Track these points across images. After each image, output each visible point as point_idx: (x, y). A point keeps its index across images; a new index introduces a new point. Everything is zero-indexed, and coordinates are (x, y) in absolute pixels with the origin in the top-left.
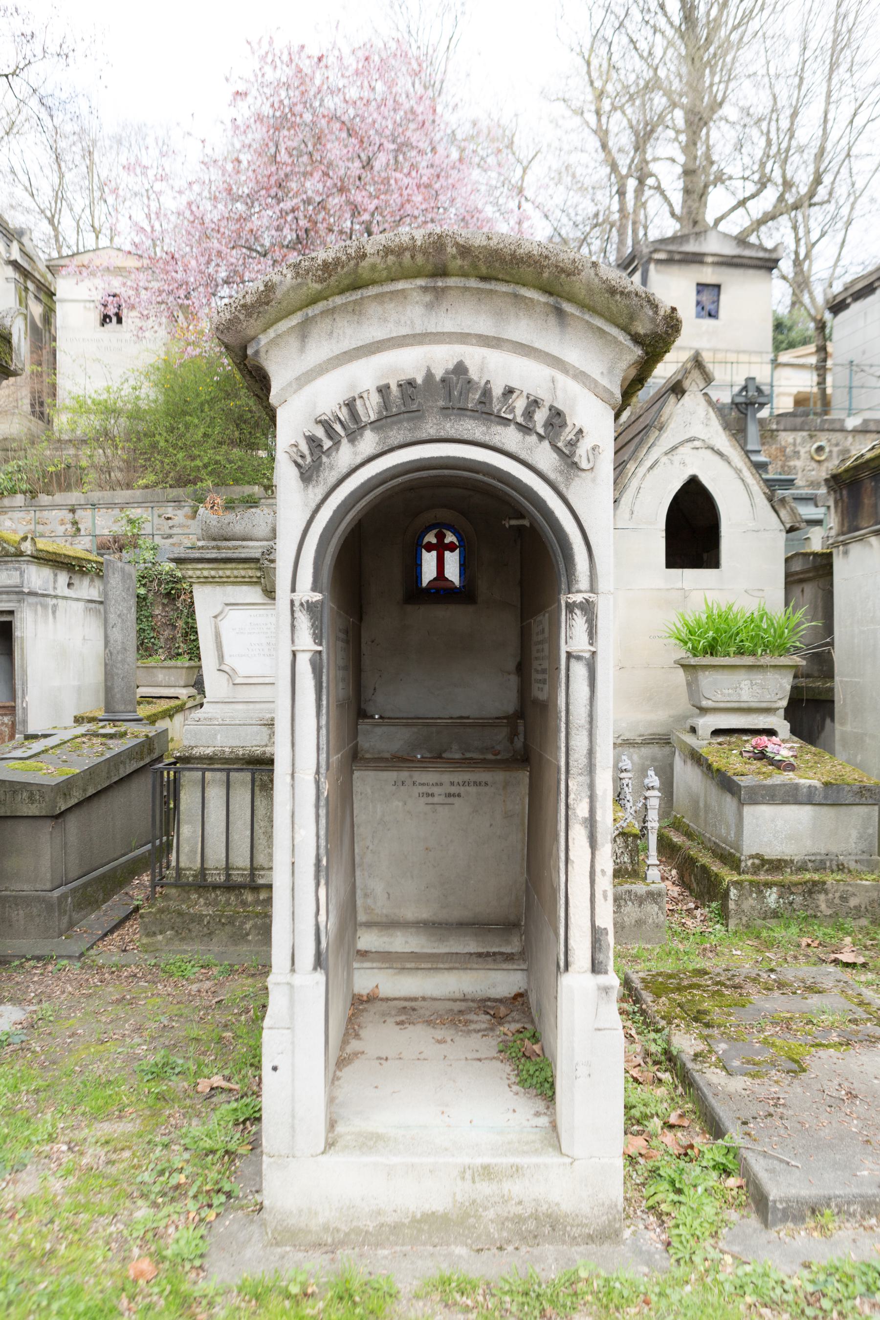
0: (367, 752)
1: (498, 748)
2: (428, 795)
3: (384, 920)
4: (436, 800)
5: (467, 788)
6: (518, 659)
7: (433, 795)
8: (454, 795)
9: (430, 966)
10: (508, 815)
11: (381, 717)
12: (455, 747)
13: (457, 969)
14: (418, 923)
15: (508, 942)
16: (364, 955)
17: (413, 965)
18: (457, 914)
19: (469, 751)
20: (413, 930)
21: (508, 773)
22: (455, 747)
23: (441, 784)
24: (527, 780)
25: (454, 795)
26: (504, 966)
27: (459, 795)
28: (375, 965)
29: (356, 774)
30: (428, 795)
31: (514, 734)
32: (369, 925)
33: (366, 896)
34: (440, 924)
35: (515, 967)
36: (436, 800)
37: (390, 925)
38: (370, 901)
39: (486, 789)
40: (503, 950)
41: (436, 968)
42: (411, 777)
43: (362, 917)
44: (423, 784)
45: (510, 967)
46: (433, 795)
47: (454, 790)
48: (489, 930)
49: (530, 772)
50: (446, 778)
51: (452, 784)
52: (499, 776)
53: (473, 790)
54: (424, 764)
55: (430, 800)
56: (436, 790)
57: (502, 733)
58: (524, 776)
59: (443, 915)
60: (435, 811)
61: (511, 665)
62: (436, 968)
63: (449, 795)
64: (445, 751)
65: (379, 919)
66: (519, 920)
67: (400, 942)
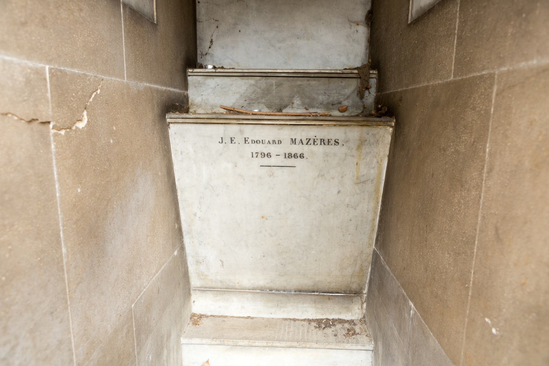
0: (200, 106)
1: (346, 103)
2: (263, 155)
3: (219, 285)
4: (273, 161)
5: (312, 147)
6: (369, 7)
7: (269, 155)
8: (295, 156)
9: (265, 344)
10: (360, 182)
11: (214, 67)
12: (297, 101)
13: (296, 347)
14: (254, 289)
15: (348, 310)
16: (196, 319)
17: (246, 342)
18: (296, 282)
19: (313, 107)
20: (250, 296)
21: (365, 129)
22: (297, 101)
23: (280, 142)
24: (388, 139)
25: (295, 156)
26: (347, 346)
27: (302, 156)
28: (204, 341)
29: (173, 130)
30: (263, 155)
31: (364, 88)
32: (204, 290)
33: (198, 262)
34: (277, 290)
35: (359, 347)
36: (273, 161)
37: (226, 290)
38: (202, 268)
39: (337, 148)
40: (343, 317)
41: (272, 346)
42: (241, 132)
43: (195, 282)
44: (257, 142)
45: (354, 347)
46: (269, 155)
47: (296, 149)
48: (329, 298)
49: (397, 123)
50: (286, 133)
51: (293, 141)
52: (354, 133)
53: (319, 149)
54: (258, 120)
55: (266, 161)
56: (273, 149)
57: (352, 86)
58: (385, 134)
59: (280, 283)
60: (271, 175)
61: (360, 13)
62: (272, 346)
63: (290, 156)
64: (285, 107)
65: (214, 285)
66: (362, 289)
67: (238, 307)
